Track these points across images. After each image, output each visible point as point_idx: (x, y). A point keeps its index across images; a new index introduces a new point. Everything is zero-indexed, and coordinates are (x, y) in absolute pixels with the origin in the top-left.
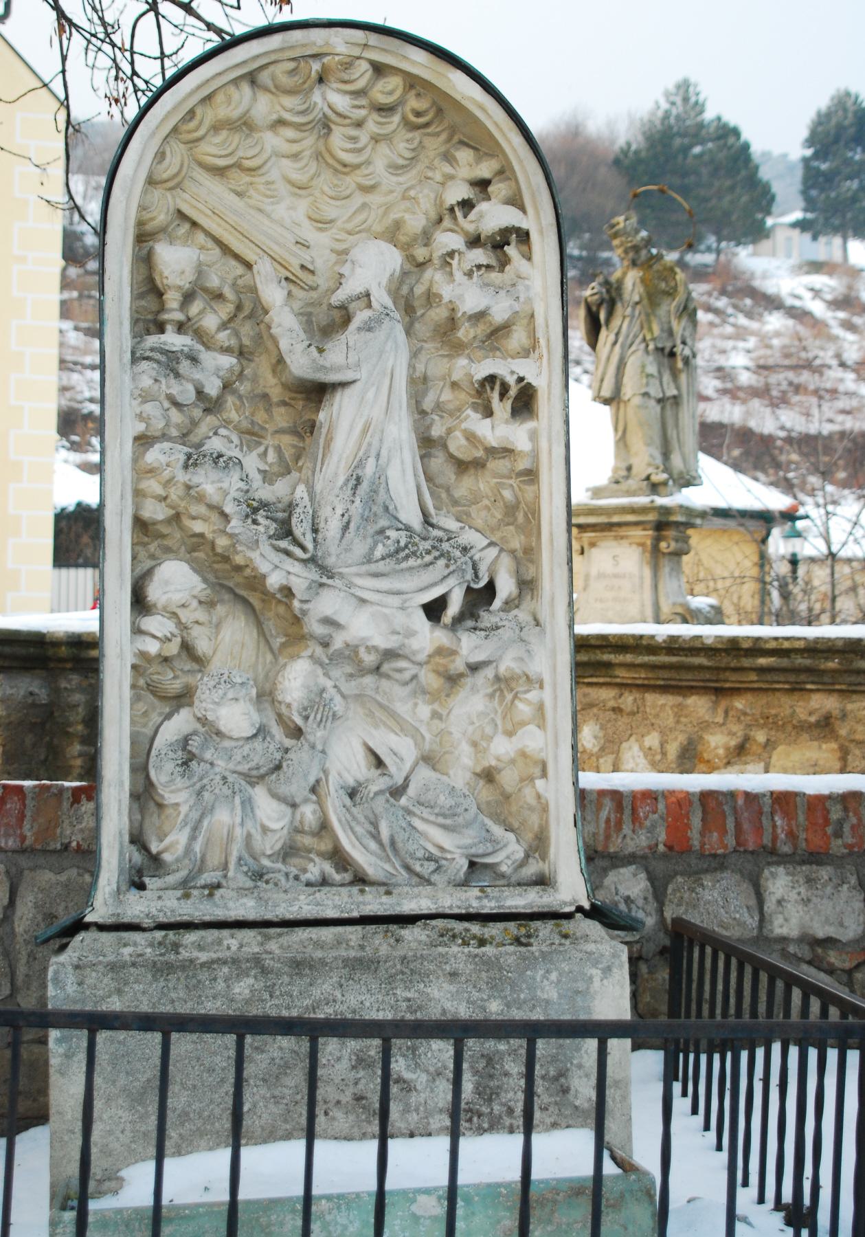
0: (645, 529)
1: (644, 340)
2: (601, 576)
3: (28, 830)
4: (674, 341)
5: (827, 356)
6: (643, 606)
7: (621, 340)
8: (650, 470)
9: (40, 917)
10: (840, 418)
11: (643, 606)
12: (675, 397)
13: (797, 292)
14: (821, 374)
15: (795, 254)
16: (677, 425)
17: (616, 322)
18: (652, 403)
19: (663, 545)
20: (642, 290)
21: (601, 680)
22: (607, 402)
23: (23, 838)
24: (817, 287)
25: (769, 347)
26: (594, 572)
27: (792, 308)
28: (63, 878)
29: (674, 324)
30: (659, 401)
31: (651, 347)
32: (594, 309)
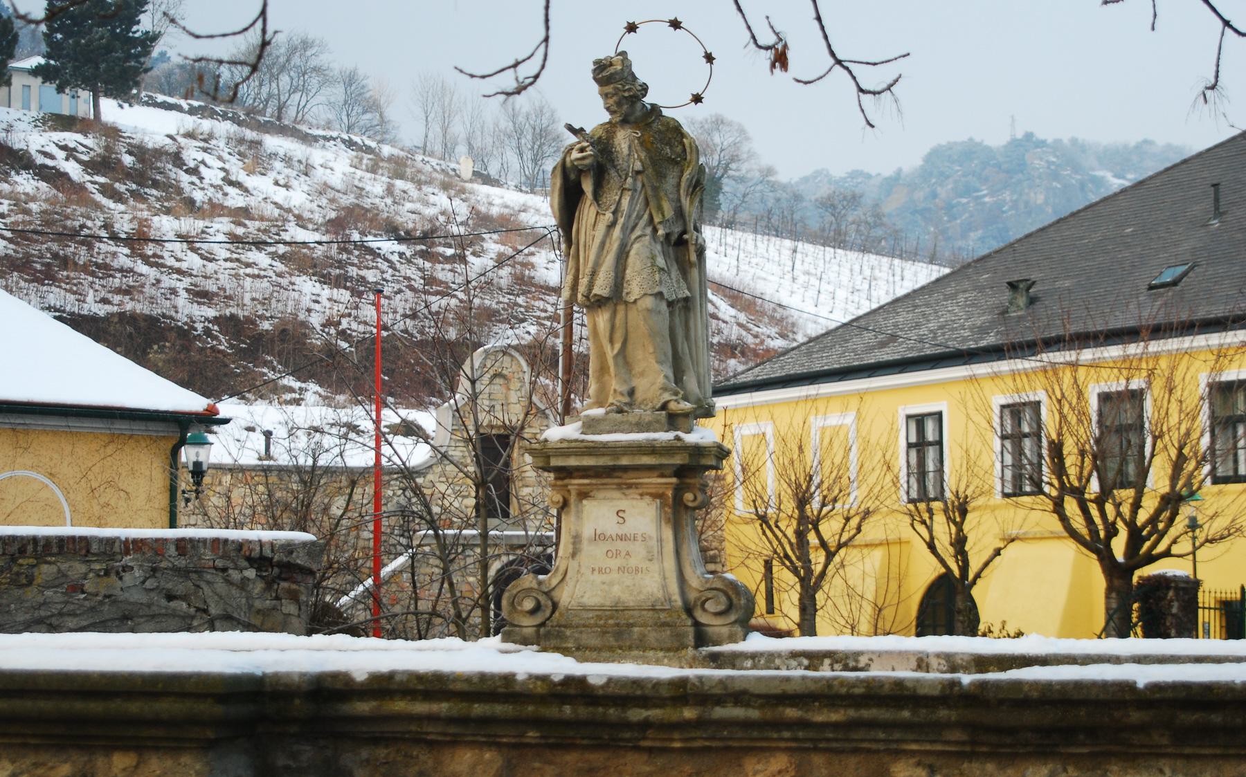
0: (662, 476)
2: (598, 537)
4: (685, 224)
5: (95, 225)
6: (665, 578)
7: (621, 221)
8: (667, 396)
10: (117, 298)
11: (665, 578)
12: (686, 299)
13: (47, 149)
14: (90, 247)
15: (34, 105)
16: (687, 337)
17: (611, 196)
19: (689, 496)
20: (643, 155)
24: (72, 145)
25: (27, 212)
26: (587, 532)
27: (44, 166)
29: (686, 202)
31: (661, 232)
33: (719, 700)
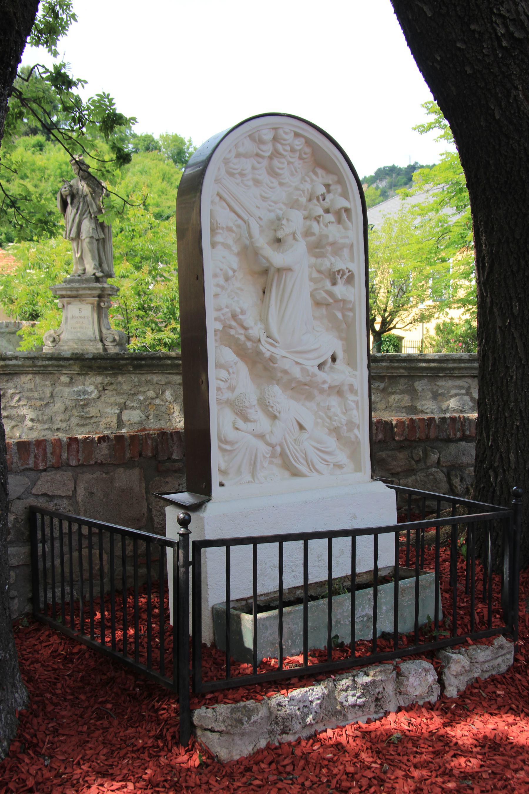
1: (90, 212)
3: (81, 457)
9: (87, 494)
12: (103, 239)
16: (104, 251)
18: (95, 241)
21: (175, 372)
22: (73, 239)
23: (79, 460)
26: (69, 316)
28: (95, 476)
30: (97, 240)
31: (93, 216)
32: (64, 197)
33: (10, 359)
